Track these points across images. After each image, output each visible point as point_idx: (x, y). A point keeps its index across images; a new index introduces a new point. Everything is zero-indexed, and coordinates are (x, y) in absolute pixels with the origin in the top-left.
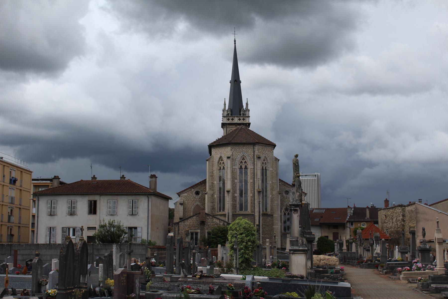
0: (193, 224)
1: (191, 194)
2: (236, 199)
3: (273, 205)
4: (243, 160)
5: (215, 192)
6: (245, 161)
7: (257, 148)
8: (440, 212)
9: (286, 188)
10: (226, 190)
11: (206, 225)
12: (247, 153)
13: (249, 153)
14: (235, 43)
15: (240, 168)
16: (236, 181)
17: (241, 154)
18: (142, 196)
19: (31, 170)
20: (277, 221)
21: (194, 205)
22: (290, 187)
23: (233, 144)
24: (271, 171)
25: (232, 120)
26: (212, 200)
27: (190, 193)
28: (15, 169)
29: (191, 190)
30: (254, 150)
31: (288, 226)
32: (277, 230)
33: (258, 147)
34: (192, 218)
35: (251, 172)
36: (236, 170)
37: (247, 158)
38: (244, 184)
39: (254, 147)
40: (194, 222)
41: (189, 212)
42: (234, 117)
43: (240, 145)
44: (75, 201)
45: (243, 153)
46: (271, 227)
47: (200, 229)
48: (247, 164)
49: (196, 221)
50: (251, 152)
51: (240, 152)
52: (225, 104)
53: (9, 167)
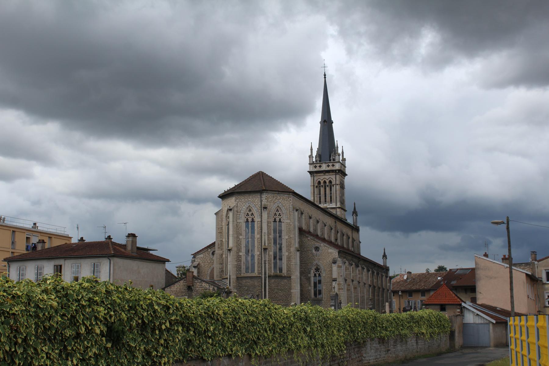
0: (180, 290)
2: (241, 259)
4: (249, 211)
5: (224, 251)
6: (252, 213)
8: (507, 267)
9: (315, 243)
10: (264, 248)
11: (195, 291)
13: (255, 203)
14: (325, 78)
15: (246, 222)
16: (241, 237)
18: (104, 259)
19: (70, 236)
20: (294, 285)
21: (211, 268)
23: (237, 194)
24: (287, 224)
25: (320, 168)
26: (221, 261)
28: (38, 235)
29: (208, 250)
31: (319, 290)
33: (267, 195)
34: (179, 282)
35: (258, 225)
37: (254, 209)
38: (251, 241)
39: (261, 196)
40: (181, 287)
41: (206, 276)
42: (322, 163)
43: (245, 195)
44: (42, 267)
45: (248, 204)
47: (187, 295)
48: (254, 216)
49: (184, 286)
52: (312, 149)
53: (25, 233)
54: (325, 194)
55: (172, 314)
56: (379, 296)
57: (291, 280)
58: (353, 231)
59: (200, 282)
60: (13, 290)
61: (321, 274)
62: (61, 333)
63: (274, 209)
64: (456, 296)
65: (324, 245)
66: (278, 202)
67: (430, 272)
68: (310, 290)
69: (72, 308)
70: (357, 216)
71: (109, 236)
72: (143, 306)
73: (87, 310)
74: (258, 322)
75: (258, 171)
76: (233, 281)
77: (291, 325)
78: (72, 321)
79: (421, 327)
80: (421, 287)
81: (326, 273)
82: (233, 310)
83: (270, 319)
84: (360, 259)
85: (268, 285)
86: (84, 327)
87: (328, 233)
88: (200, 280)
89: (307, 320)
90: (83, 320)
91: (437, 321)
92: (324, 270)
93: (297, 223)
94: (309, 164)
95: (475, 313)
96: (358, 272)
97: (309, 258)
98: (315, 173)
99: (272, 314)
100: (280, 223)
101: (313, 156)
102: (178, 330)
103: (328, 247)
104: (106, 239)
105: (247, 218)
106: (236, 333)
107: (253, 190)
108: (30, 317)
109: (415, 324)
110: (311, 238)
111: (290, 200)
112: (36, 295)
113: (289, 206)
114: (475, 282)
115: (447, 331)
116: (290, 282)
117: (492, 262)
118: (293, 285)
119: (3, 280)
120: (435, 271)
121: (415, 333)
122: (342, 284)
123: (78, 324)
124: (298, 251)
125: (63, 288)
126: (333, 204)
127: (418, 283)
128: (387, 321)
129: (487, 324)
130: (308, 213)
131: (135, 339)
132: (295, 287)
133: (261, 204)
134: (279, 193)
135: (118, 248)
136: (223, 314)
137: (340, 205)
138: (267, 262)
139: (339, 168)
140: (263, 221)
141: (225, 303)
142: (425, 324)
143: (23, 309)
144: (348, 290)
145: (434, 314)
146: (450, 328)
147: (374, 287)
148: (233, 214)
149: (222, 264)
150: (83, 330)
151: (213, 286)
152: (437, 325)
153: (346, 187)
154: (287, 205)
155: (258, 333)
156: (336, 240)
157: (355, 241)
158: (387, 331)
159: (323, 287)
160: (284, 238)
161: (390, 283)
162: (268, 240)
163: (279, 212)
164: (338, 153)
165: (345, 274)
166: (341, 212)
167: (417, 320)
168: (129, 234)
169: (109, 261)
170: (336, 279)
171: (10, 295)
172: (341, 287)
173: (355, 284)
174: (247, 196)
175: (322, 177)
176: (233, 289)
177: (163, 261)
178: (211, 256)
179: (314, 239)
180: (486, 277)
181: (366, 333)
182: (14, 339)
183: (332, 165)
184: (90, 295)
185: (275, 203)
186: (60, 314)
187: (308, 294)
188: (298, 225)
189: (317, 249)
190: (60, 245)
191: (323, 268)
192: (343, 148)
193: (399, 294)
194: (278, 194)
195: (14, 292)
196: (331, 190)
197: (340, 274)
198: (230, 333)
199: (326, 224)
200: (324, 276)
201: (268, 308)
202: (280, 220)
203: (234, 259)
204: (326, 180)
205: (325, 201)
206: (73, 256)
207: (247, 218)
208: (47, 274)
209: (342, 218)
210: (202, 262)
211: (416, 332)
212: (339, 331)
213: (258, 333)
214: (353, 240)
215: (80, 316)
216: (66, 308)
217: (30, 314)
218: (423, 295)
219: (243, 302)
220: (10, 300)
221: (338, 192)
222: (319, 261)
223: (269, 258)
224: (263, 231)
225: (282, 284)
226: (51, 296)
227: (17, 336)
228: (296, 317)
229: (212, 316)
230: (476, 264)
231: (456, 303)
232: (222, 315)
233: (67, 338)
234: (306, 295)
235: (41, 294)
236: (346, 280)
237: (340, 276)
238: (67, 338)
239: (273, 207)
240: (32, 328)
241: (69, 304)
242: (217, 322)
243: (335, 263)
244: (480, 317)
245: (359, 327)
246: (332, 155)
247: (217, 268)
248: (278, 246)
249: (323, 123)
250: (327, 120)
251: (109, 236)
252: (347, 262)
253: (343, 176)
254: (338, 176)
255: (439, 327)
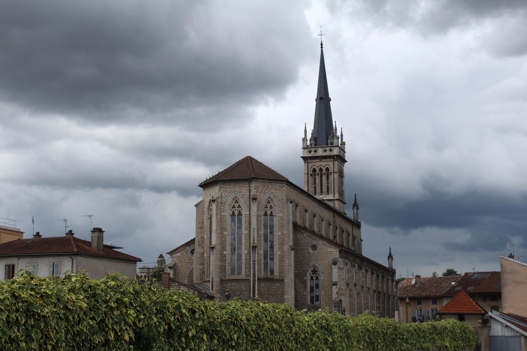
1: (185, 254)
2: (225, 258)
3: (283, 266)
4: (235, 203)
5: (205, 250)
6: (239, 205)
7: (254, 185)
10: (253, 245)
12: (240, 193)
14: (322, 47)
15: (232, 215)
16: (225, 233)
17: (233, 195)
18: (65, 258)
19: (21, 231)
20: (288, 289)
21: (189, 269)
22: (319, 240)
23: (221, 182)
24: (279, 218)
25: (316, 153)
27: (184, 252)
29: (186, 248)
30: (249, 188)
31: (316, 296)
32: (289, 301)
33: (256, 184)
35: (246, 219)
36: (226, 218)
39: (249, 185)
42: (318, 147)
43: (231, 183)
46: (280, 297)
48: (241, 209)
50: (246, 192)
51: (232, 193)
52: (306, 131)
54: (321, 183)
55: (199, 319)
56: (384, 303)
57: (284, 284)
58: (354, 227)
59: (178, 285)
60: (41, 288)
61: (319, 277)
62: (90, 340)
63: (265, 201)
64: (477, 303)
65: (322, 242)
66: (270, 193)
67: (437, 276)
68: (306, 296)
69: (102, 311)
70: (359, 209)
71: (71, 231)
72: (170, 310)
73: (115, 313)
74: (281, 330)
75: (246, 156)
76: (216, 285)
77: (313, 334)
78: (101, 325)
79: (444, 340)
80: (432, 294)
81: (325, 275)
82: (257, 316)
83: (293, 327)
84: (363, 260)
85: (257, 289)
86: (113, 332)
87: (326, 229)
88: (178, 283)
89: (327, 329)
90: (112, 324)
91: (462, 333)
92: (322, 272)
93: (291, 217)
94: (303, 148)
95: (504, 324)
96: (361, 275)
97: (305, 258)
98: (309, 159)
99: (294, 321)
100: (272, 217)
101: (307, 139)
102: (202, 337)
103: (327, 245)
104: (67, 234)
105: (233, 211)
106: (259, 343)
107: (240, 178)
108: (60, 320)
109: (438, 335)
110: (307, 235)
111: (284, 191)
112: (64, 295)
113: (282, 196)
114: (500, 288)
115: (472, 345)
116: (282, 286)
117: (521, 264)
118: (287, 289)
119: (28, 276)
120: (443, 275)
121: (438, 347)
122: (344, 289)
123: (107, 329)
124: (292, 249)
125: (90, 287)
126: (330, 195)
127: (429, 288)
128: (408, 332)
129: (518, 337)
130: (303, 206)
131: (162, 347)
132: (289, 292)
133: (250, 194)
134: (271, 182)
135: (81, 244)
136: (246, 320)
137: (338, 197)
138: (256, 262)
139: (337, 153)
140: (252, 214)
141: (248, 308)
142: (448, 336)
143: (53, 311)
144: (350, 296)
145: (458, 324)
146: (476, 341)
147: (379, 293)
148: (217, 206)
149: (203, 264)
150: (112, 336)
151: (193, 290)
152: (461, 338)
153: (345, 175)
154: (280, 196)
155: (281, 343)
156: (335, 237)
157: (356, 238)
158: (407, 343)
159: (322, 293)
160: (276, 235)
161: (397, 288)
162: (257, 236)
163: (270, 204)
164: (336, 136)
165: (347, 277)
166: (340, 205)
167: (440, 331)
168: (94, 229)
169: (71, 260)
170: (336, 283)
171: (38, 293)
172: (342, 293)
173: (357, 289)
174: (233, 185)
175: (318, 164)
176: (216, 294)
177: (134, 260)
178: (190, 255)
179: (311, 236)
180: (514, 282)
181: (386, 346)
182: (44, 346)
183: (329, 149)
184: (118, 295)
185: (265, 194)
186: (89, 316)
187: (304, 301)
188: (292, 220)
189: (314, 247)
190: (12, 242)
191: (321, 269)
192: (342, 130)
193: (406, 301)
194: (270, 182)
195: (42, 290)
196: (328, 179)
197: (341, 277)
198: (253, 342)
199: (323, 219)
200: (322, 280)
201: (290, 314)
202: (271, 213)
203: (217, 259)
204: (322, 167)
205: (321, 192)
206: (29, 254)
207: (233, 211)
208: (69, 271)
209: (341, 212)
210: (179, 262)
211: (439, 345)
212: (358, 342)
213: (281, 343)
214: (354, 238)
215: (109, 319)
216: (95, 310)
217: (60, 316)
218: (434, 303)
219: (265, 307)
220: (40, 300)
221: (336, 182)
222: (316, 261)
223: (258, 257)
224: (252, 227)
225: (273, 288)
226: (80, 296)
227: (47, 341)
228: (317, 325)
229: (235, 322)
230: (502, 266)
231: (478, 312)
232: (245, 322)
233: (95, 345)
234: (301, 302)
235: (68, 294)
236: (348, 284)
237: (341, 279)
238: (95, 345)
239: (263, 198)
240: (62, 334)
241: (98, 305)
242: (240, 329)
243: (335, 265)
244: (509, 329)
245: (379, 338)
246: (330, 138)
247: (197, 269)
248: (269, 243)
249: (320, 100)
250: (324, 97)
251: (71, 230)
252: (348, 262)
253: (342, 163)
254: (336, 163)
255: (464, 340)
